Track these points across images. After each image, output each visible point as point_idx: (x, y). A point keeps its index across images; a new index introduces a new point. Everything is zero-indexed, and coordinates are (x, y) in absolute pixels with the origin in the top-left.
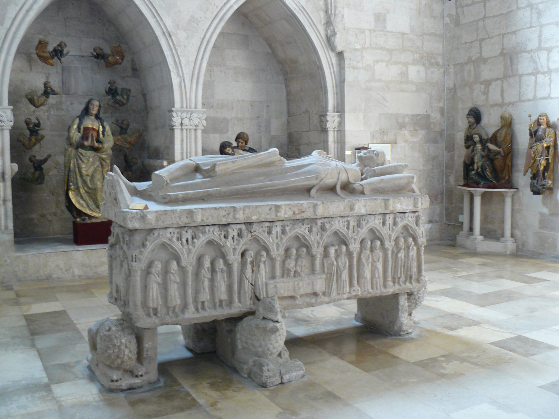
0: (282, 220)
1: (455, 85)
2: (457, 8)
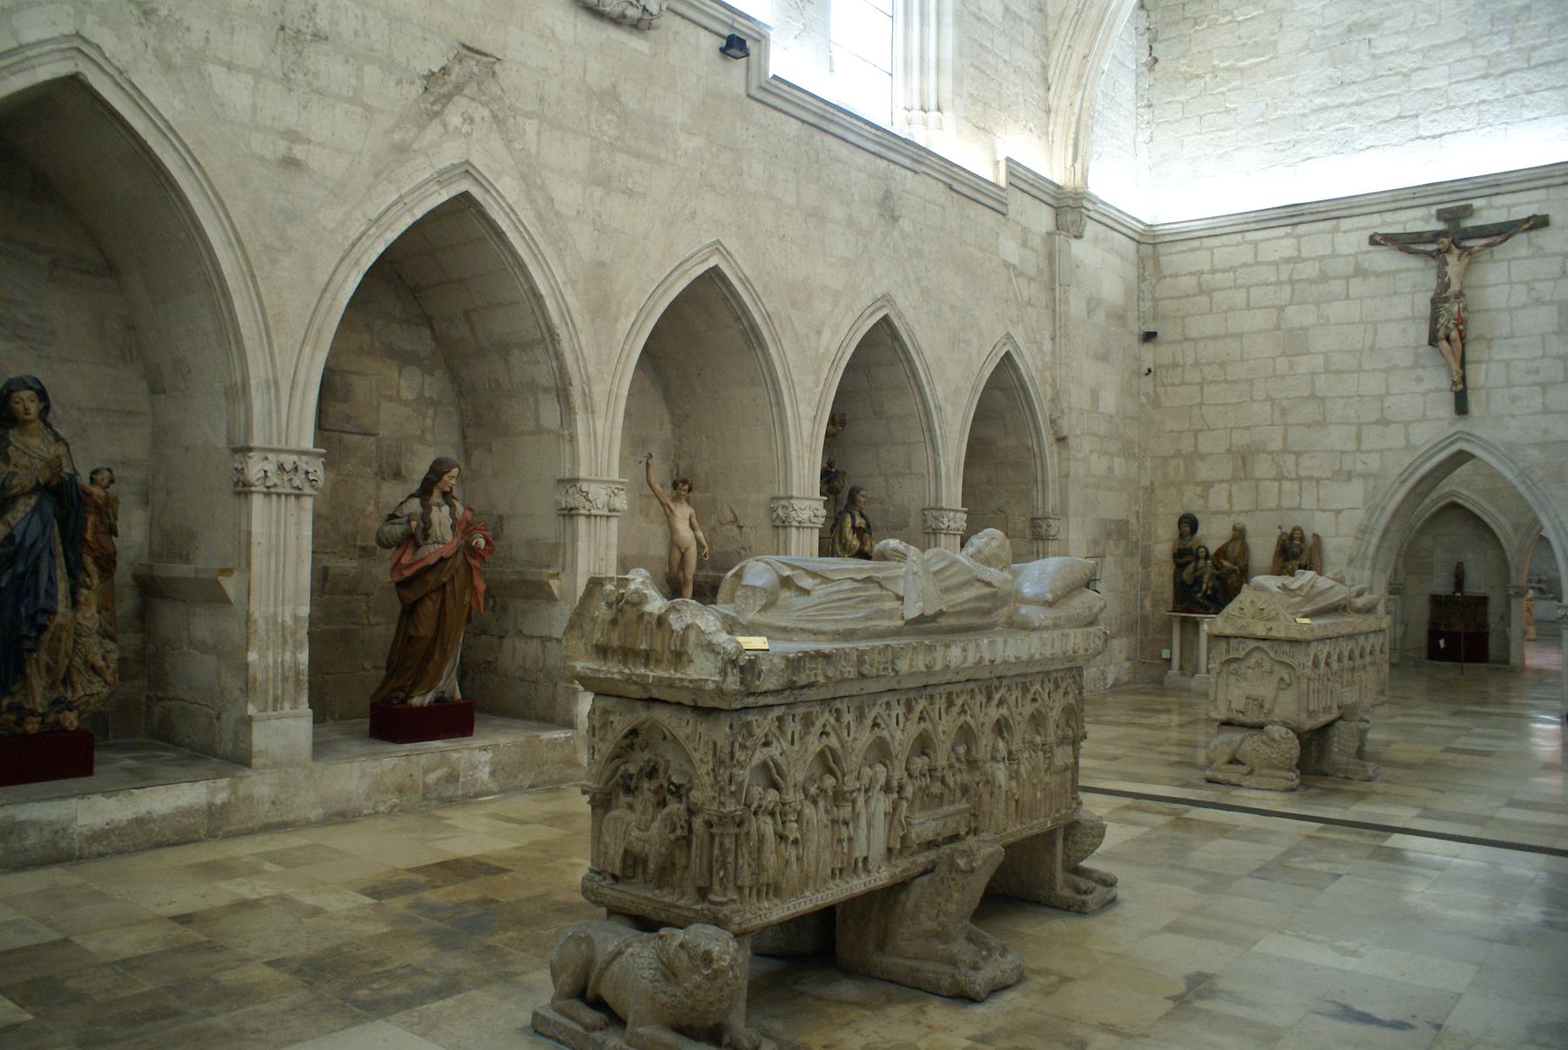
0: (623, 700)
1: (1152, 483)
2: (1155, 386)
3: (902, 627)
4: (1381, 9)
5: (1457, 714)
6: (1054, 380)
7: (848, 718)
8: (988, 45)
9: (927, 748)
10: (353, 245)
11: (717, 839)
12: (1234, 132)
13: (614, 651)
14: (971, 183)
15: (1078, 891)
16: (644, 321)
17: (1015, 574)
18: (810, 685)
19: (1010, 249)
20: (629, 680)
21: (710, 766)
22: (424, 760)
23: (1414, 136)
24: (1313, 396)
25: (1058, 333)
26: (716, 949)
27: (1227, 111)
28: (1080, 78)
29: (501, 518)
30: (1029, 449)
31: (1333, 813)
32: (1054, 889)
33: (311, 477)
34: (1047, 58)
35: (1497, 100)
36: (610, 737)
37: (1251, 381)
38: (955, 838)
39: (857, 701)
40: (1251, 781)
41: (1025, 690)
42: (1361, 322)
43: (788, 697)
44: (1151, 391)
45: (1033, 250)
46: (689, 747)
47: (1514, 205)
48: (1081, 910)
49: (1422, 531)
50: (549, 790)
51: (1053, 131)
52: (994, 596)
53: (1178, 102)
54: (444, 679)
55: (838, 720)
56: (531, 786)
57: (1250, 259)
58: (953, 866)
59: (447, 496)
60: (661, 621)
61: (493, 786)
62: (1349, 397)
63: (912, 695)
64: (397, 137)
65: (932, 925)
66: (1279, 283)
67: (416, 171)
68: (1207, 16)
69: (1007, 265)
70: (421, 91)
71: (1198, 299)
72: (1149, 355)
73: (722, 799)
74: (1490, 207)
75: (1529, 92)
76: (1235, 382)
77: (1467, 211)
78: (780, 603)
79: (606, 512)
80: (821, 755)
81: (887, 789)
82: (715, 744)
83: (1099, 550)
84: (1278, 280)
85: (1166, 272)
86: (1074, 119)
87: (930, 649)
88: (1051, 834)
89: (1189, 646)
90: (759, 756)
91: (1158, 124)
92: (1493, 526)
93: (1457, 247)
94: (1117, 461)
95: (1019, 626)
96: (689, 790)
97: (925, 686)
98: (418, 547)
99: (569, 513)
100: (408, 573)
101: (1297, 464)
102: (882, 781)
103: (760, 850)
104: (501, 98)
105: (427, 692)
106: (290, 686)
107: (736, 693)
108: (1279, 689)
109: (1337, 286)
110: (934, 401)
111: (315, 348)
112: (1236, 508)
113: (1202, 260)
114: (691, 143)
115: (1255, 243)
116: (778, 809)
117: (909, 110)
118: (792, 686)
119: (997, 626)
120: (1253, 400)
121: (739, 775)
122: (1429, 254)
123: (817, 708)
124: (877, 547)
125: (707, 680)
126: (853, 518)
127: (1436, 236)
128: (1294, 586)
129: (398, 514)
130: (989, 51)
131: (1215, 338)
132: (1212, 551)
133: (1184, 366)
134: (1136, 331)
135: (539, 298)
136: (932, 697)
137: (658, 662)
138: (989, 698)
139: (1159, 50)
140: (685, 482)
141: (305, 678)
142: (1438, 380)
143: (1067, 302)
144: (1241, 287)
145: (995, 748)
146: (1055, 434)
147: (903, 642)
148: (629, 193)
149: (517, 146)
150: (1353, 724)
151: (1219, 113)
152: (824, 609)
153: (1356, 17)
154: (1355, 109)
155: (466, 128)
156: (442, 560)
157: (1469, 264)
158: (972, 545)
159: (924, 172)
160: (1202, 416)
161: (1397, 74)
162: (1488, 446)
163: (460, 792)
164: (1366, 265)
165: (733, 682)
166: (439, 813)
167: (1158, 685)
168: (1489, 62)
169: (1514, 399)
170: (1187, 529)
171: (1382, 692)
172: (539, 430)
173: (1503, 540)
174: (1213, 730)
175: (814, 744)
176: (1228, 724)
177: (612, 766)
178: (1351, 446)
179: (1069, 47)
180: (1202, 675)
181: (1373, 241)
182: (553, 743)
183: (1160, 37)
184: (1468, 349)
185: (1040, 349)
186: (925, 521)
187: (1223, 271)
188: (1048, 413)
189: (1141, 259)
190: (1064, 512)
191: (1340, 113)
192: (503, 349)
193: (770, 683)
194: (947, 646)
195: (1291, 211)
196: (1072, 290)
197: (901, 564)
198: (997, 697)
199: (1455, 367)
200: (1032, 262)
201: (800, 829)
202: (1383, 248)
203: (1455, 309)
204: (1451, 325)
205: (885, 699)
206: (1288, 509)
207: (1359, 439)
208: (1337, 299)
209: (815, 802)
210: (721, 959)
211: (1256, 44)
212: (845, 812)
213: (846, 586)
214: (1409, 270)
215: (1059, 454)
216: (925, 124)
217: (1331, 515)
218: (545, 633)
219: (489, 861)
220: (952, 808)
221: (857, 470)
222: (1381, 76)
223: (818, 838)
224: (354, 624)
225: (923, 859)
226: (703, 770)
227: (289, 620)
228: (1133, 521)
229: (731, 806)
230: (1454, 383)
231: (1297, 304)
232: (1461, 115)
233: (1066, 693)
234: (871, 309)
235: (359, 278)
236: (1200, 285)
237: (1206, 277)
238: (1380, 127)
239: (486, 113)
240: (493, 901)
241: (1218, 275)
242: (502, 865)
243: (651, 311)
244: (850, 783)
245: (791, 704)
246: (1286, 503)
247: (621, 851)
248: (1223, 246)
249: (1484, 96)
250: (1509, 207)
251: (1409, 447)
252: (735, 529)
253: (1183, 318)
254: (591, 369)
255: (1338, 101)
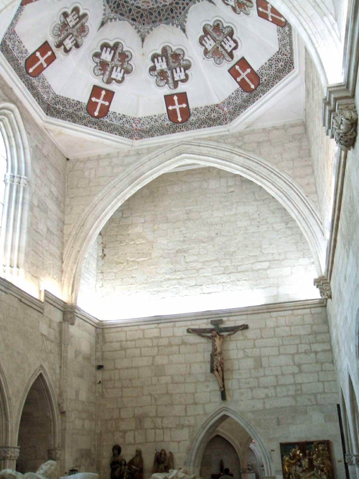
1: (101, 432)
4: (188, 246)
6: (60, 386)
8: (40, 243)
12: (135, 286)
14: (29, 300)
23: (201, 293)
24: (167, 393)
25: (62, 366)
27: (132, 277)
28: (76, 259)
30: (48, 417)
34: (63, 250)
35: (228, 282)
37: (142, 387)
44: (100, 390)
45: (53, 329)
47: (237, 320)
51: (64, 280)
53: (113, 272)
62: (181, 394)
66: (153, 347)
68: (125, 241)
69: (42, 335)
71: (121, 352)
74: (228, 320)
75: (238, 281)
77: (221, 321)
84: (153, 345)
86: (73, 276)
91: (105, 280)
92: (232, 444)
93: (219, 335)
94: (87, 422)
109: (175, 349)
110: (7, 395)
112: (137, 442)
113: (122, 336)
115: (143, 330)
117: (5, 266)
122: (209, 337)
127: (211, 331)
130: (40, 245)
131: (127, 368)
132: (127, 461)
133: (114, 380)
134: (95, 365)
139: (106, 251)
142: (214, 386)
143: (67, 352)
146: (60, 410)
151: (129, 278)
153: (180, 247)
154: (180, 281)
158: (42, 469)
159: (10, 294)
160: (122, 401)
161: (195, 269)
162: (234, 412)
164: (186, 340)
168: (225, 268)
169: (242, 394)
170: (117, 452)
173: (236, 449)
178: (183, 414)
179: (72, 247)
181: (188, 331)
183: (107, 247)
184: (225, 374)
185: (55, 373)
187: (131, 341)
188: (57, 400)
189: (97, 335)
190: (63, 447)
191: (175, 282)
195: (157, 318)
196: (69, 347)
199: (221, 381)
200: (53, 334)
202: (192, 334)
203: (219, 359)
204: (218, 365)
208: (175, 354)
211: (144, 253)
214: (202, 343)
215: (61, 419)
216: (11, 272)
222: (189, 270)
228: (93, 449)
230: (221, 388)
231: (160, 355)
232: (217, 286)
236: (121, 346)
237: (124, 343)
238: (189, 288)
241: (129, 343)
249: (224, 280)
250: (235, 321)
251: (205, 414)
255: (174, 277)
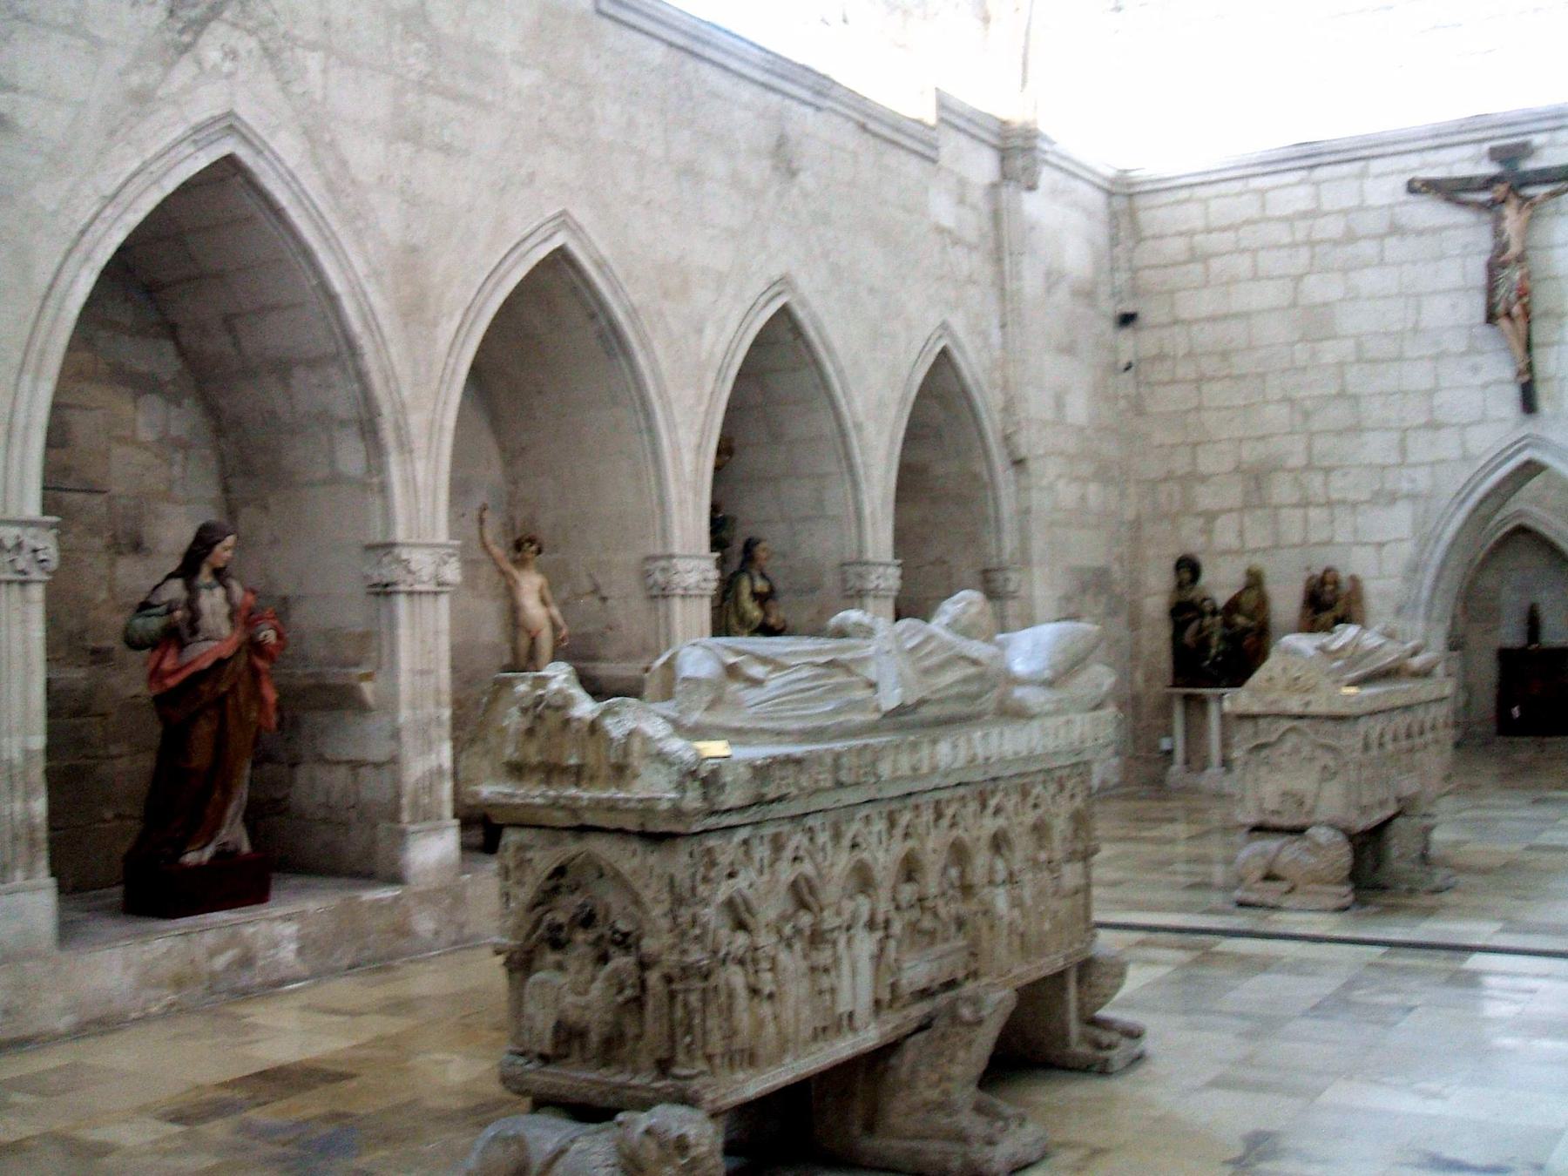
0: (543, 831)
3: (879, 720)
5: (1536, 802)
7: (823, 838)
9: (915, 871)
10: (83, 233)
11: (680, 997)
13: (534, 769)
15: (1098, 1046)
16: (472, 325)
17: (1002, 646)
18: (780, 799)
19: (943, 209)
20: (554, 804)
21: (666, 906)
22: (210, 938)
24: (1341, 395)
26: (691, 1131)
29: (285, 600)
30: (976, 477)
31: (1397, 933)
32: (1067, 1045)
33: (42, 557)
36: (530, 878)
37: (1262, 376)
38: (951, 984)
39: (832, 816)
40: (1289, 902)
41: (1025, 793)
42: (1400, 295)
43: (753, 815)
45: (974, 207)
46: (637, 885)
48: (1103, 1070)
49: (1484, 565)
50: (379, 969)
52: (981, 677)
54: (227, 826)
55: (811, 840)
56: (350, 967)
57: (1253, 212)
58: (955, 1019)
59: (220, 575)
60: (594, 727)
61: (301, 968)
63: (895, 805)
64: (135, 80)
65: (934, 1095)
66: (1294, 245)
67: (164, 127)
69: (940, 230)
70: (165, 15)
72: (1128, 344)
73: (686, 946)
74: (1551, 144)
76: (1243, 377)
78: (728, 697)
79: (432, 587)
80: (794, 886)
81: (871, 925)
82: (672, 879)
83: (1072, 609)
85: (1148, 232)
87: (915, 746)
88: (1061, 975)
89: (1195, 734)
90: (724, 890)
94: (1093, 488)
95: (1015, 714)
96: (639, 938)
97: (910, 794)
98: (182, 646)
99: (384, 591)
100: (171, 682)
101: (1326, 484)
102: (865, 917)
103: (730, 1008)
104: (272, 23)
105: (206, 845)
106: (22, 847)
107: (697, 812)
108: (1323, 780)
109: (1368, 249)
111: (36, 379)
113: (1192, 216)
114: (524, 79)
115: (1262, 192)
116: (749, 956)
118: (760, 801)
119: (986, 714)
120: (1267, 402)
121: (704, 915)
122: (1482, 207)
123: (786, 828)
124: (834, 621)
125: (659, 799)
126: (752, 579)
127: (1489, 183)
128: (1335, 646)
129: (155, 601)
131: (1212, 319)
135: (332, 298)
136: (917, 807)
137: (592, 779)
138: (984, 806)
140: (532, 541)
141: (42, 834)
142: (1499, 368)
144: (1243, 251)
145: (992, 870)
147: (885, 739)
148: (446, 149)
149: (296, 89)
150: (1416, 820)
152: (783, 703)
155: (227, 66)
156: (220, 663)
157: (1531, 217)
158: (945, 612)
163: (259, 980)
164: (1404, 221)
165: (693, 799)
166: (231, 1009)
167: (1157, 786)
170: (1187, 576)
171: (1447, 778)
172: (335, 479)
174: (1240, 837)
175: (786, 872)
176: (1260, 829)
177: (534, 916)
178: (1394, 458)
180: (1215, 770)
181: (1412, 188)
182: (378, 906)
186: (844, 581)
187: (1223, 229)
189: (1114, 217)
190: (1025, 561)
192: (282, 368)
193: (733, 798)
194: (934, 742)
195: (1306, 150)
197: (868, 642)
198: (993, 803)
199: (1519, 351)
200: (972, 224)
201: (776, 981)
205: (864, 811)
206: (1317, 544)
207: (1403, 451)
209: (789, 946)
210: (697, 1145)
212: (823, 957)
213: (805, 673)
214: (1456, 226)
217: (1370, 551)
218: (354, 753)
219: (324, 1066)
220: (947, 947)
221: (753, 515)
223: (797, 990)
224: (87, 757)
225: (918, 1011)
226: (657, 911)
227: (17, 755)
228: (1116, 567)
229: (696, 955)
233: (1072, 796)
234: (765, 297)
235: (93, 278)
237: (1198, 238)
239: (253, 43)
240: (346, 1115)
241: (1214, 236)
242: (343, 1069)
243: (480, 310)
244: (830, 920)
245: (757, 823)
246: (1315, 537)
247: (551, 1023)
248: (1217, 197)
251: (1466, 458)
252: (597, 603)
253: (1172, 292)
254: (406, 392)
